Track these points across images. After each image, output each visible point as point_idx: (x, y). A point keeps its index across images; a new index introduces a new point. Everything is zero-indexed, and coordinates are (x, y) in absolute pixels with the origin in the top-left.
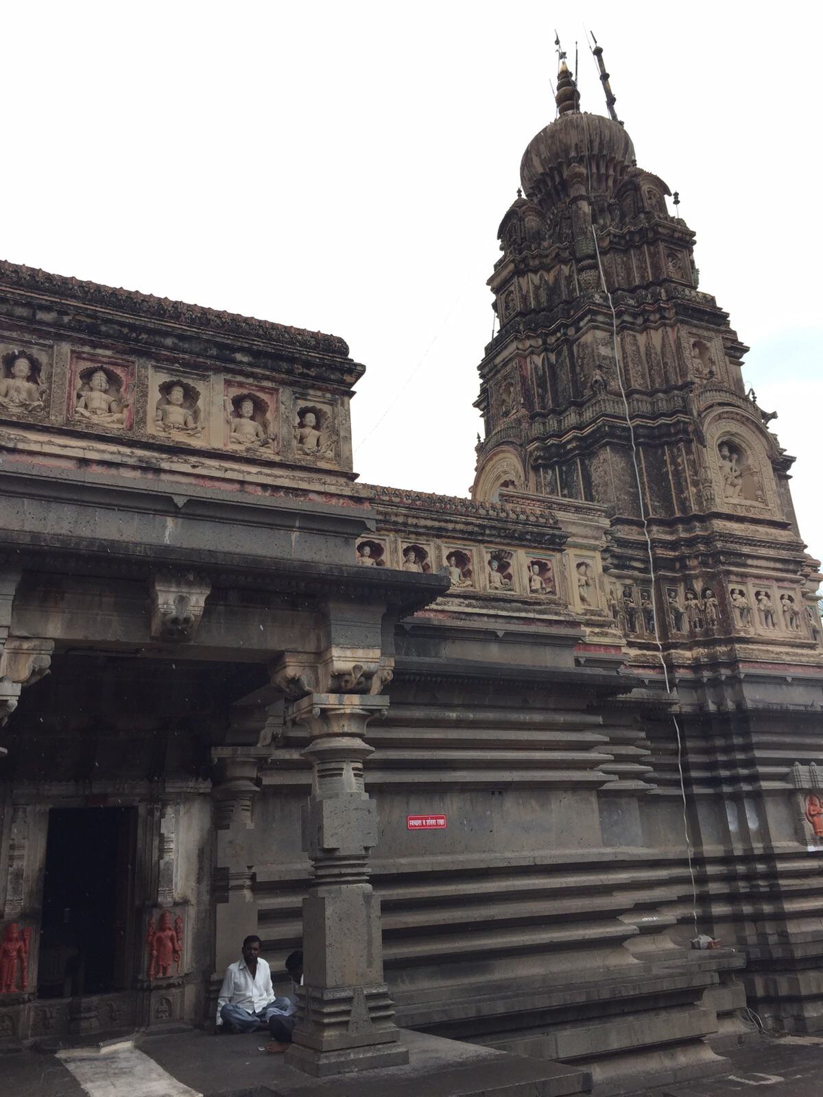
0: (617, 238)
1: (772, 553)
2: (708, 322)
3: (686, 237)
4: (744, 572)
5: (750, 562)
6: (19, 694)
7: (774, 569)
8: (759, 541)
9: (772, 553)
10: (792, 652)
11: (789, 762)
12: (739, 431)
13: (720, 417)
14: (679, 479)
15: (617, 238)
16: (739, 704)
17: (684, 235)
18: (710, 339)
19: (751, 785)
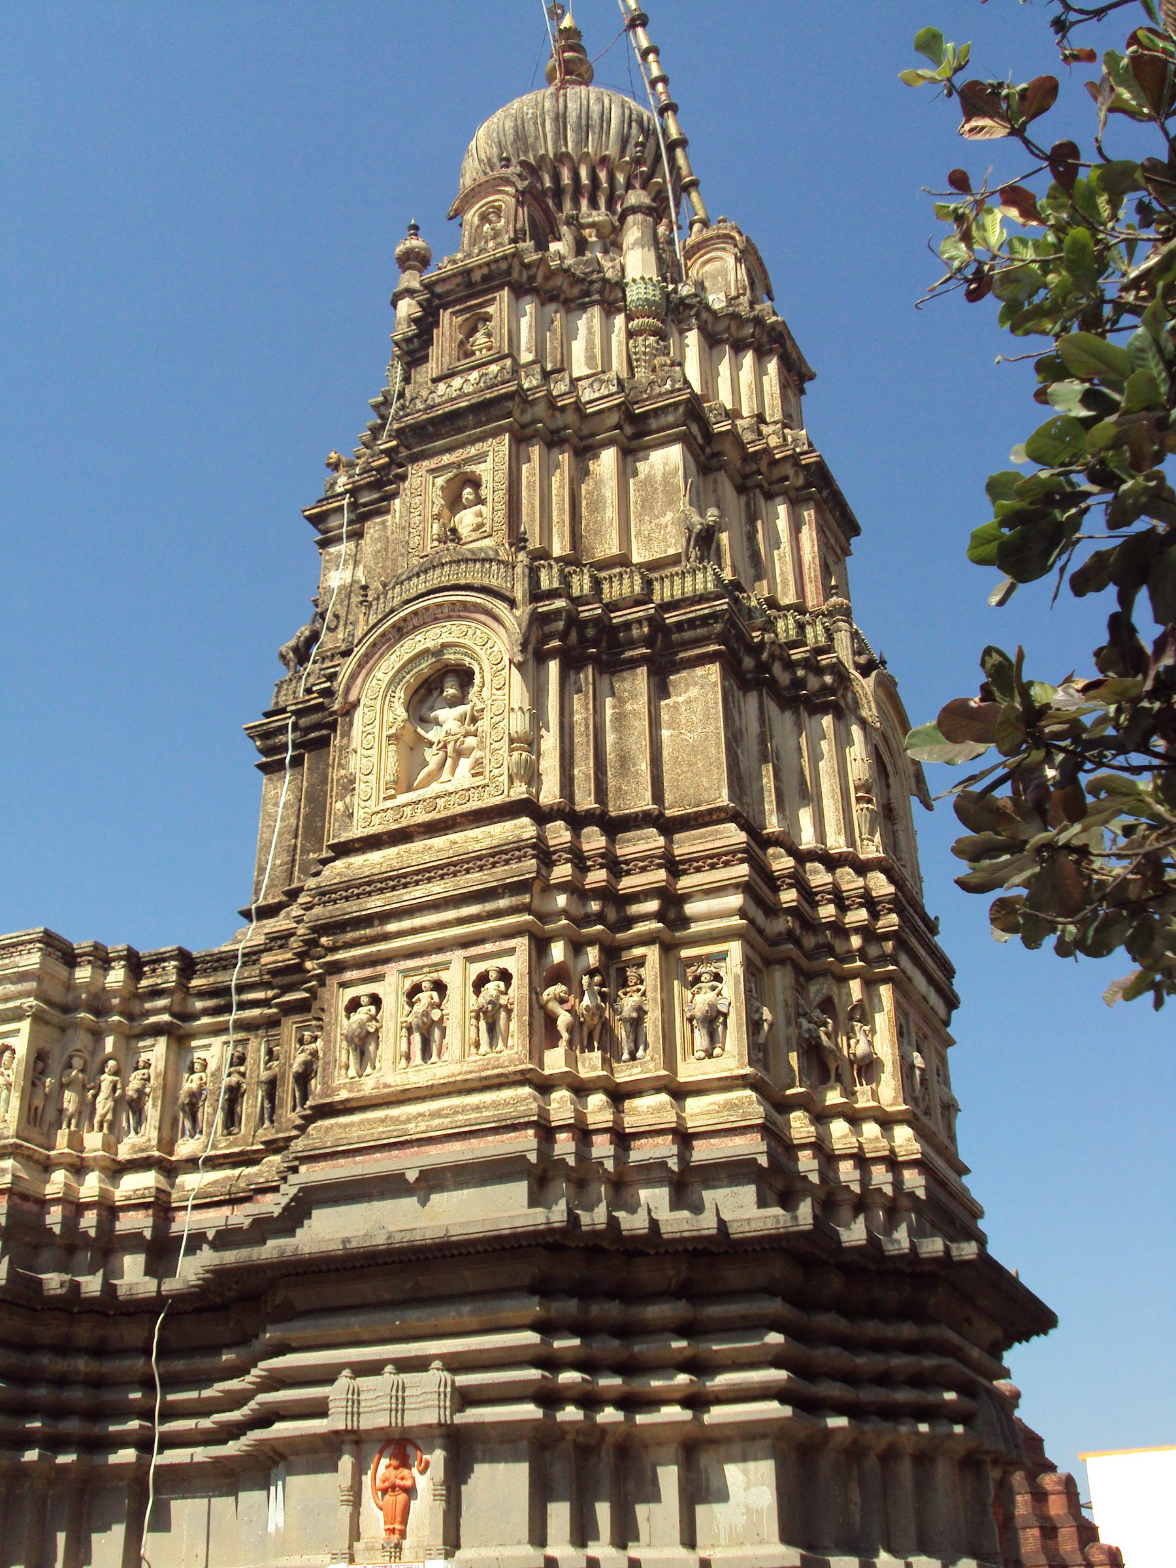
0: (416, 341)
1: (438, 889)
2: (480, 424)
3: (498, 268)
4: (370, 954)
5: (392, 927)
6: (535, 1146)
7: (461, 921)
8: (417, 872)
9: (438, 889)
10: (450, 1108)
11: (327, 1376)
12: (445, 639)
13: (400, 630)
14: (620, 738)
15: (416, 341)
16: (109, 1289)
17: (493, 267)
18: (481, 458)
19: (632, 1356)
